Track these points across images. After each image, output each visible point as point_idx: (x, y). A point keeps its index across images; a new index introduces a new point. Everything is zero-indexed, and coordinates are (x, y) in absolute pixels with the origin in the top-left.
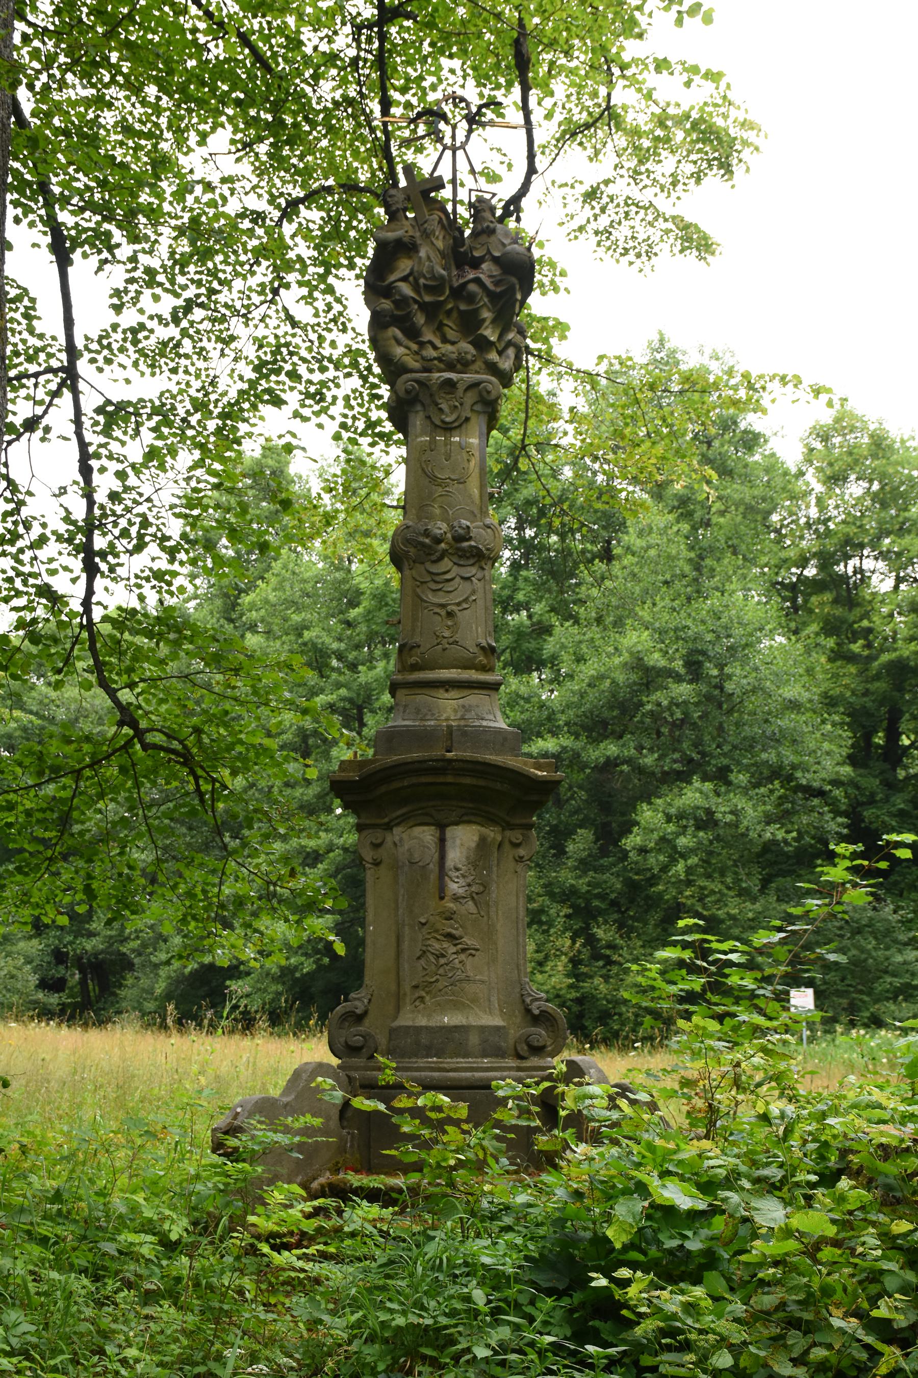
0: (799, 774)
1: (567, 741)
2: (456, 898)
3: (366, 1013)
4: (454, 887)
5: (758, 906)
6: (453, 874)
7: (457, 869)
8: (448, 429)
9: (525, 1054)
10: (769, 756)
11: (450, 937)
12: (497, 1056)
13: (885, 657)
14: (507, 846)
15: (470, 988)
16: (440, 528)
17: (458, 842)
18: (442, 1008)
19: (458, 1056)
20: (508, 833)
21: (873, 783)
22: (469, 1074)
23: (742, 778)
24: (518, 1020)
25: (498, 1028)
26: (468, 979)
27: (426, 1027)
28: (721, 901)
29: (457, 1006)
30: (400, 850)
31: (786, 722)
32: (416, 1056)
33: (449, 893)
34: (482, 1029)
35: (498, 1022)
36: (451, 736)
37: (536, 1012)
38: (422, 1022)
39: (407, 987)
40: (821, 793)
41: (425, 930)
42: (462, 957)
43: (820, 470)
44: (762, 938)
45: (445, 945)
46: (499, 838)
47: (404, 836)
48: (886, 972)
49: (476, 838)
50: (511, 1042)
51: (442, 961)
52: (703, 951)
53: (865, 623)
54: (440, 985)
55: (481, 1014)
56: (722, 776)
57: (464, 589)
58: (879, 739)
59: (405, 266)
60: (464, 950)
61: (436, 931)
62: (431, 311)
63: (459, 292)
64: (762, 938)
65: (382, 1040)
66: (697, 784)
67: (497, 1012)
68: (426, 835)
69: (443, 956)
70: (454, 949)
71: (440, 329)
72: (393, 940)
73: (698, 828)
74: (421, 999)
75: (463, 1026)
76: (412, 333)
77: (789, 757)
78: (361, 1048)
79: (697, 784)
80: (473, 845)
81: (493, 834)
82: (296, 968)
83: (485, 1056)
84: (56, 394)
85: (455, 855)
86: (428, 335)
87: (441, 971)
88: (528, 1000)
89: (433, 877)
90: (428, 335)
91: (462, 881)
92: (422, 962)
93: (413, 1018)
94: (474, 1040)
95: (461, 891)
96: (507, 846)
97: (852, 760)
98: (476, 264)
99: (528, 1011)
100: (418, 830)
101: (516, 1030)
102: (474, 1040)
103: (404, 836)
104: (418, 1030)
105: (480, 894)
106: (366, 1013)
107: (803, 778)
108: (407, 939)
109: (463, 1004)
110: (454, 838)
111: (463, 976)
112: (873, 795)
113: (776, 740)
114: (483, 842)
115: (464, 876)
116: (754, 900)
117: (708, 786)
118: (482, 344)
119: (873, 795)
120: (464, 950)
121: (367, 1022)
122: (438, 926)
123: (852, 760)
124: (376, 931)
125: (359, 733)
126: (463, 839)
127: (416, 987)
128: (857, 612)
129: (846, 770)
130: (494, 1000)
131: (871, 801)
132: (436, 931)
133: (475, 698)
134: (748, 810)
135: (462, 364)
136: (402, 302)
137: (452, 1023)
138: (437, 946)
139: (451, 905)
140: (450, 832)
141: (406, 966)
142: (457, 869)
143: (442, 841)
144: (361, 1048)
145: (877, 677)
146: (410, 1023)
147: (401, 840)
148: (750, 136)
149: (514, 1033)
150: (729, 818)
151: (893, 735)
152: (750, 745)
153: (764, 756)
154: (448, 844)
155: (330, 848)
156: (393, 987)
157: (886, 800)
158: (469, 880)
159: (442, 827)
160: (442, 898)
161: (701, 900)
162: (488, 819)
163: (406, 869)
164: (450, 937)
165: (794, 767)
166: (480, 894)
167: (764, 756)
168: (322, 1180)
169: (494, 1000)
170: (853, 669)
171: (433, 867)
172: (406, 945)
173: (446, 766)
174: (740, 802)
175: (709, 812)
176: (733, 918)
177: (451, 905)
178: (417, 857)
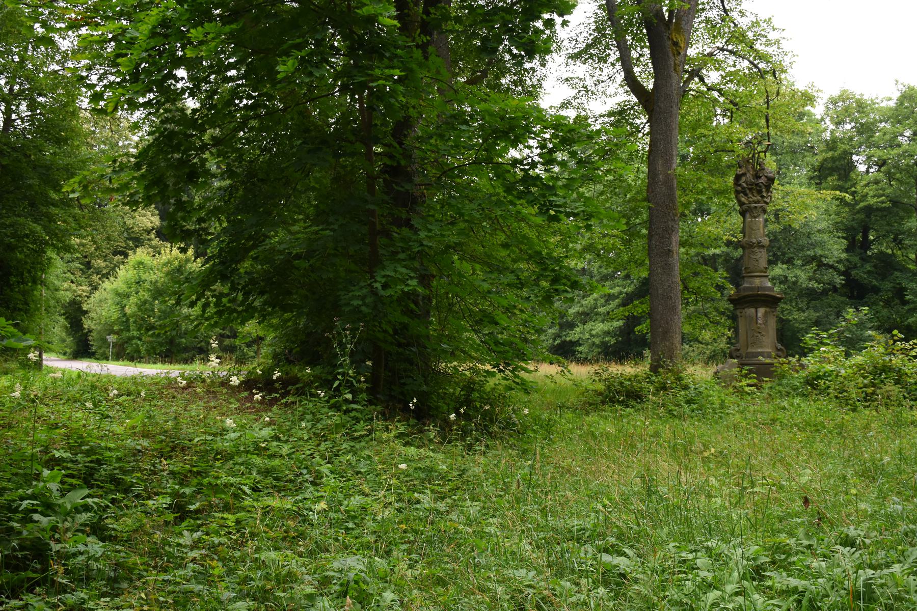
0: (823, 259)
1: (725, 249)
4: (760, 322)
5: (806, 314)
8: (755, 217)
10: (811, 253)
13: (862, 204)
16: (754, 241)
18: (757, 348)
21: (855, 259)
23: (799, 262)
28: (790, 313)
29: (761, 347)
31: (816, 238)
36: (758, 288)
40: (832, 267)
43: (832, 118)
44: (831, 332)
48: (861, 340)
52: (817, 335)
53: (853, 189)
56: (789, 261)
57: (760, 255)
58: (859, 237)
59: (744, 179)
62: (750, 190)
63: (757, 185)
64: (831, 332)
65: (744, 355)
66: (780, 265)
68: (753, 310)
71: (752, 193)
73: (780, 283)
76: (746, 195)
77: (819, 252)
79: (780, 265)
81: (768, 309)
82: (608, 342)
85: (760, 315)
86: (750, 195)
90: (750, 195)
97: (847, 250)
98: (760, 177)
105: (765, 323)
107: (825, 261)
112: (856, 264)
113: (813, 246)
114: (766, 312)
116: (804, 311)
117: (785, 266)
118: (763, 197)
119: (856, 264)
123: (847, 250)
124: (742, 330)
126: (761, 311)
128: (849, 183)
129: (844, 256)
131: (855, 267)
133: (763, 279)
134: (802, 275)
135: (758, 202)
136: (743, 188)
143: (756, 312)
145: (858, 212)
148: (820, 94)
150: (794, 279)
151: (865, 236)
152: (802, 249)
153: (809, 253)
155: (621, 293)
157: (862, 266)
159: (756, 308)
161: (782, 312)
162: (767, 306)
165: (821, 256)
166: (765, 323)
167: (809, 253)
170: (847, 209)
173: (758, 295)
174: (798, 272)
175: (786, 277)
176: (795, 319)
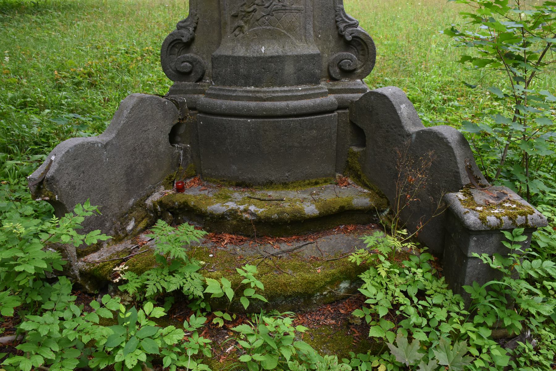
3: (192, 40)
9: (338, 77)
12: (311, 83)
18: (259, 37)
19: (274, 85)
22: (283, 104)
24: (332, 44)
25: (312, 57)
26: (284, 9)
27: (244, 58)
29: (275, 35)
32: (236, 84)
34: (297, 58)
35: (313, 49)
37: (349, 38)
38: (241, 52)
39: (227, 17)
50: (325, 65)
54: (257, 15)
55: (297, 43)
67: (312, 39)
74: (240, 27)
75: (279, 57)
78: (190, 73)
83: (299, 83)
84: (544, 64)
88: (342, 26)
93: (234, 48)
94: (289, 69)
99: (341, 36)
101: (331, 54)
102: (289, 69)
104: (237, 59)
106: (192, 40)
109: (280, 34)
111: (279, 6)
121: (194, 47)
127: (235, 16)
130: (310, 27)
137: (269, 54)
144: (190, 73)
146: (229, 53)
149: (327, 58)
156: (216, 15)
168: (156, 197)
169: (310, 27)
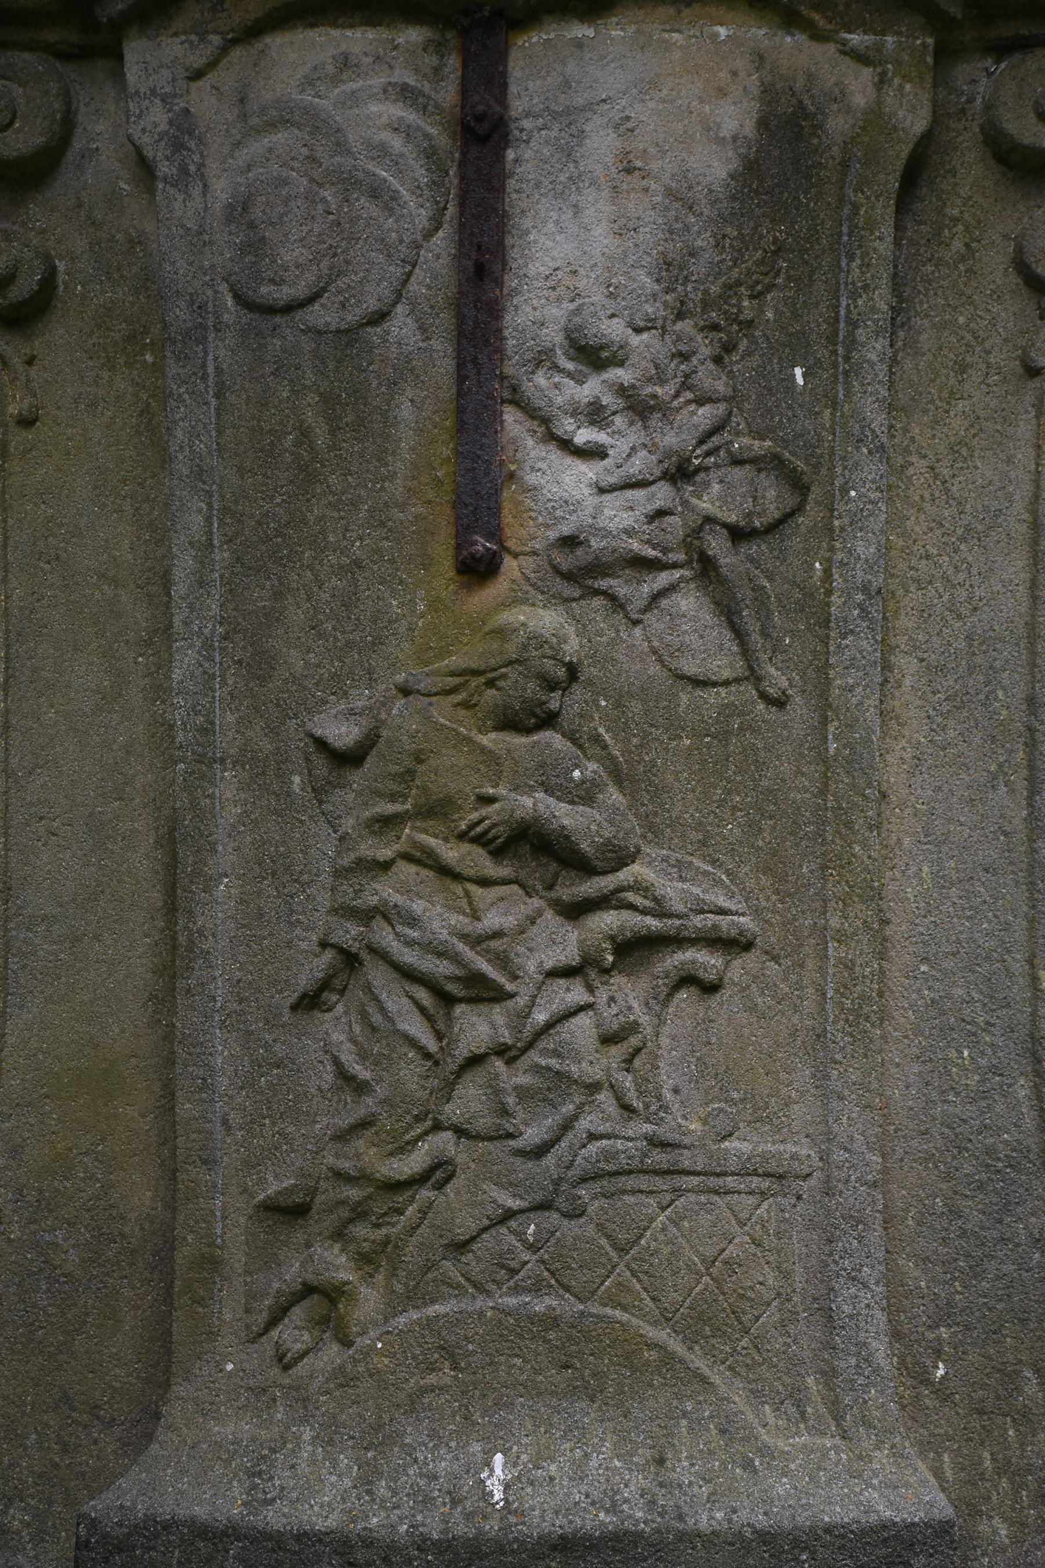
2: (582, 570)
4: (569, 488)
6: (565, 390)
7: (593, 356)
11: (535, 848)
14: (968, 172)
15: (687, 1232)
17: (601, 145)
20: (979, 78)
26: (664, 1163)
29: (587, 1367)
30: (182, 208)
33: (528, 533)
38: (321, 1493)
41: (355, 799)
42: (628, 995)
45: (499, 914)
46: (911, 115)
47: (205, 102)
49: (736, 117)
51: (477, 1028)
54: (459, 1207)
55: (767, 1425)
60: (634, 949)
61: (436, 810)
69: (483, 992)
70: (565, 943)
72: (142, 861)
74: (325, 1298)
80: (715, 167)
85: (579, 251)
87: (469, 1101)
89: (416, 417)
91: (625, 444)
92: (337, 1027)
95: (620, 518)
96: (968, 172)
100: (300, 56)
103: (205, 102)
105: (755, 544)
108: (225, 857)
110: (570, 118)
111: (629, 1141)
115: (640, 408)
120: (634, 949)
122: (451, 773)
125: (707, 1269)
127: (290, 1211)
132: (436, 810)
137: (544, 1515)
138: (439, 917)
139: (546, 619)
140: (542, 65)
141: (223, 1052)
142: (593, 356)
143: (481, 138)
147: (184, 131)
154: (528, 160)
156: (138, 1195)
158: (675, 437)
160: (477, 570)
163: (220, 351)
164: (535, 848)
166: (755, 544)
169: (863, 1304)
171: (416, 337)
172: (220, 906)
177: (546, 619)
178: (293, 261)
